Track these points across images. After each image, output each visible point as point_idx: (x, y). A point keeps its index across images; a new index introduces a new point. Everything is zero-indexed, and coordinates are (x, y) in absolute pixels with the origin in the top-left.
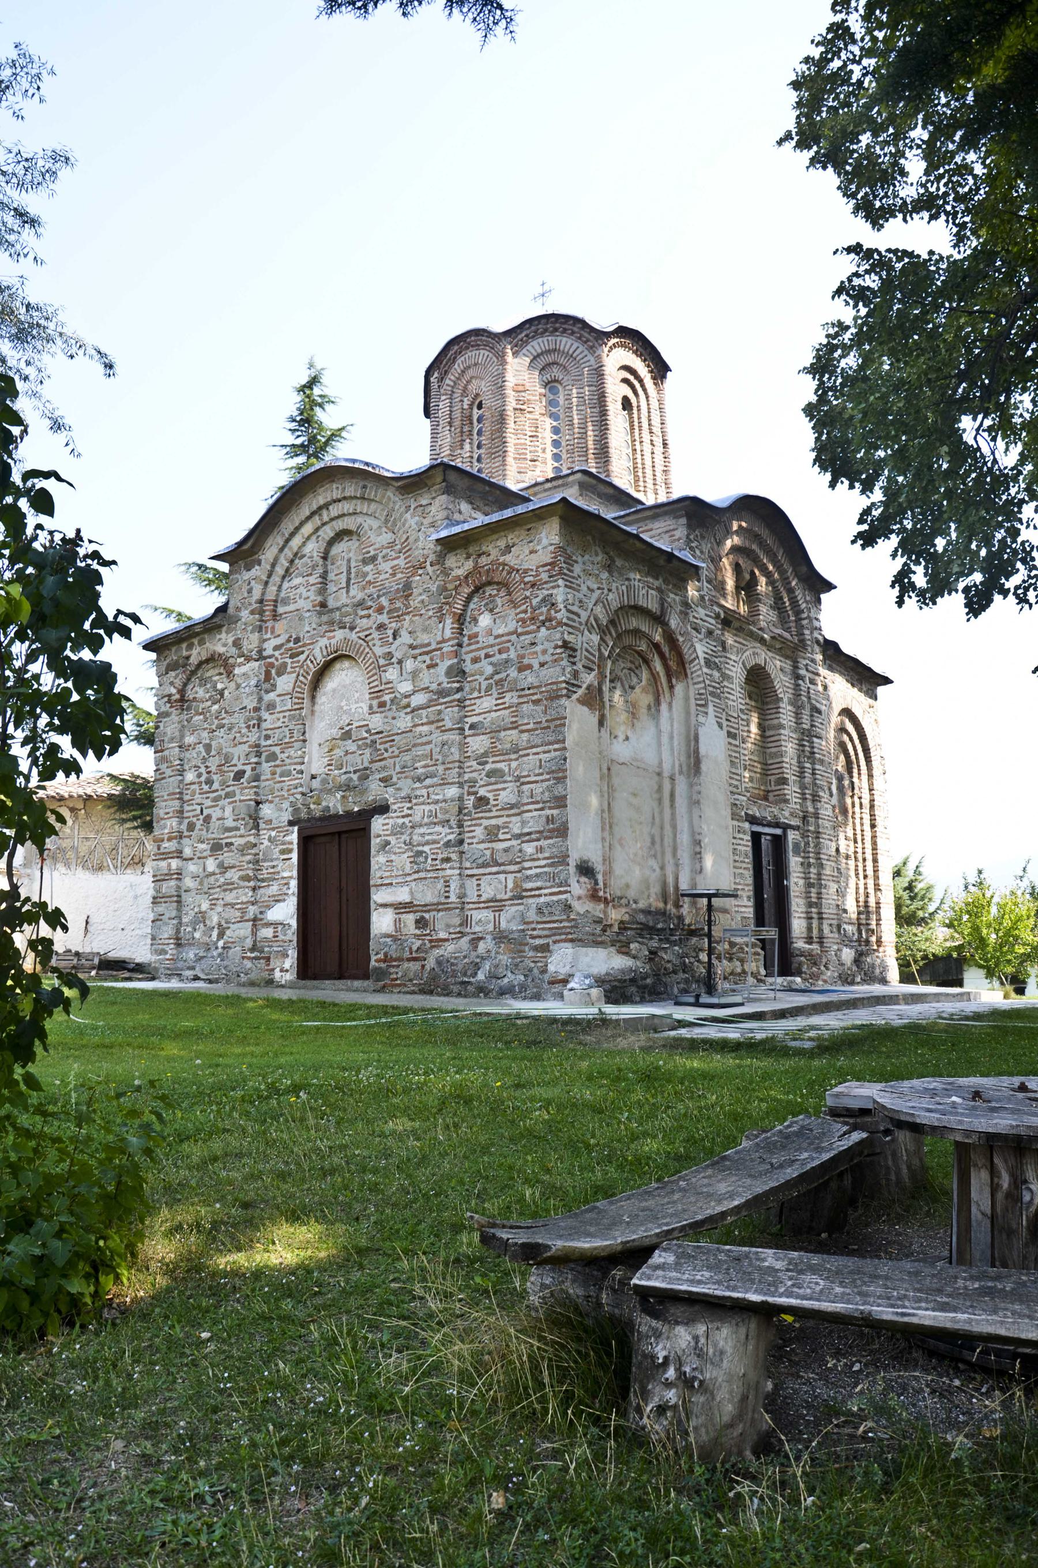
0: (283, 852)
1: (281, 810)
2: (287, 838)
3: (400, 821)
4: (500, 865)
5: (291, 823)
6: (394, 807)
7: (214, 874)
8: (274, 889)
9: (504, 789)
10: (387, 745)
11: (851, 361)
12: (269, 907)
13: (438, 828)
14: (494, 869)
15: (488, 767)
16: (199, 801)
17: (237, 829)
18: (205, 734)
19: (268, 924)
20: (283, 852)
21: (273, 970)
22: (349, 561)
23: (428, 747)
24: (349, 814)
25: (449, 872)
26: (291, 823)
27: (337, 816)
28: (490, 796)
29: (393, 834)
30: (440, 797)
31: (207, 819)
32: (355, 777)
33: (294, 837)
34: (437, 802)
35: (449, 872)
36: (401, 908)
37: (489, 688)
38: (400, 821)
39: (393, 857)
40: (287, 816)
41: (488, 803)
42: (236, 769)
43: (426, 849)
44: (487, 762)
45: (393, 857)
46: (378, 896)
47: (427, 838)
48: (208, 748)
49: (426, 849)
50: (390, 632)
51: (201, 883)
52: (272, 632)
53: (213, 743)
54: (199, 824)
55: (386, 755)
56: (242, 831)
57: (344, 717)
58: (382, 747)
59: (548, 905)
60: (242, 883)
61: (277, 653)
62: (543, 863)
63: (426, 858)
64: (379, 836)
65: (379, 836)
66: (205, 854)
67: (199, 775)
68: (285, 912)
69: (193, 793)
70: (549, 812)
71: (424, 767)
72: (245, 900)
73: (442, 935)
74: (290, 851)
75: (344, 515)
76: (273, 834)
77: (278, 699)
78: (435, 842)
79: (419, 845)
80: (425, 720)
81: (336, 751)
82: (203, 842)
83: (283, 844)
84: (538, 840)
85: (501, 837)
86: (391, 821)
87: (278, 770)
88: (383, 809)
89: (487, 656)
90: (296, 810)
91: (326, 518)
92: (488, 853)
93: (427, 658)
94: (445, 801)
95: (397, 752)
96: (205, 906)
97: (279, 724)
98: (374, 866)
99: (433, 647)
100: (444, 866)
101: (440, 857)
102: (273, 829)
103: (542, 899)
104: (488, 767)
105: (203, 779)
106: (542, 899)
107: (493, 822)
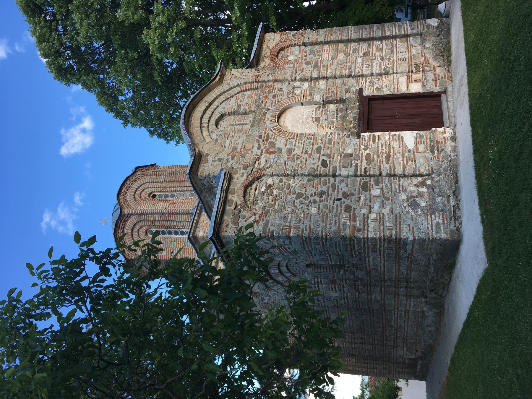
0: (374, 141)
1: (350, 144)
2: (367, 138)
3: (368, 83)
4: (393, 46)
5: (359, 137)
6: (360, 86)
7: (382, 189)
8: (395, 144)
9: (362, 47)
10: (330, 91)
11: (159, 288)
12: (406, 147)
13: (374, 64)
14: (395, 48)
15: (351, 52)
16: (332, 201)
17: (356, 165)
18: (289, 197)
19: (417, 148)
20: (374, 141)
21: (444, 138)
22: (230, 125)
23: (338, 69)
24: (359, 108)
25: (395, 58)
26: (359, 137)
27: (360, 114)
28: (363, 52)
29: (373, 86)
30: (361, 64)
31: (345, 195)
32: (340, 114)
33: (366, 135)
34: (363, 65)
35: (395, 58)
36: (409, 80)
37: (319, 55)
38: (368, 83)
39: (384, 85)
40: (355, 140)
41: (367, 52)
42: (320, 166)
43: (383, 67)
44: (349, 53)
45: (384, 85)
46: (403, 90)
47: (378, 68)
48: (299, 196)
49: (383, 67)
50: (279, 92)
51: (388, 199)
52: (249, 150)
53: (298, 191)
54: (348, 202)
55: (335, 92)
56: (359, 162)
57: (308, 120)
58: (330, 93)
59: (410, 27)
60: (391, 161)
61: (262, 148)
62: (394, 29)
63: (387, 67)
64: (373, 91)
65: (373, 91)
66: (368, 197)
67: (315, 202)
68: (409, 137)
69: (325, 206)
70: (375, 29)
71: (346, 70)
72: (401, 158)
73: (423, 59)
74: (374, 136)
75: (210, 118)
76: (363, 147)
77: (288, 147)
78: (380, 64)
79: (381, 70)
80: (325, 71)
81: (324, 125)
82: (360, 198)
83: (369, 140)
84: (385, 31)
85: (381, 47)
86: (367, 87)
87: (327, 145)
88: (361, 90)
89: (306, 56)
90: (352, 134)
91: (206, 125)
92: (387, 51)
93: (298, 72)
94: (363, 62)
95: (335, 87)
96: (403, 196)
97: (301, 146)
98: (388, 93)
99: (294, 71)
100: (392, 61)
101: (387, 62)
102: (360, 147)
103: (409, 28)
104: (351, 52)
105: (317, 199)
106: (409, 28)
107: (374, 50)
